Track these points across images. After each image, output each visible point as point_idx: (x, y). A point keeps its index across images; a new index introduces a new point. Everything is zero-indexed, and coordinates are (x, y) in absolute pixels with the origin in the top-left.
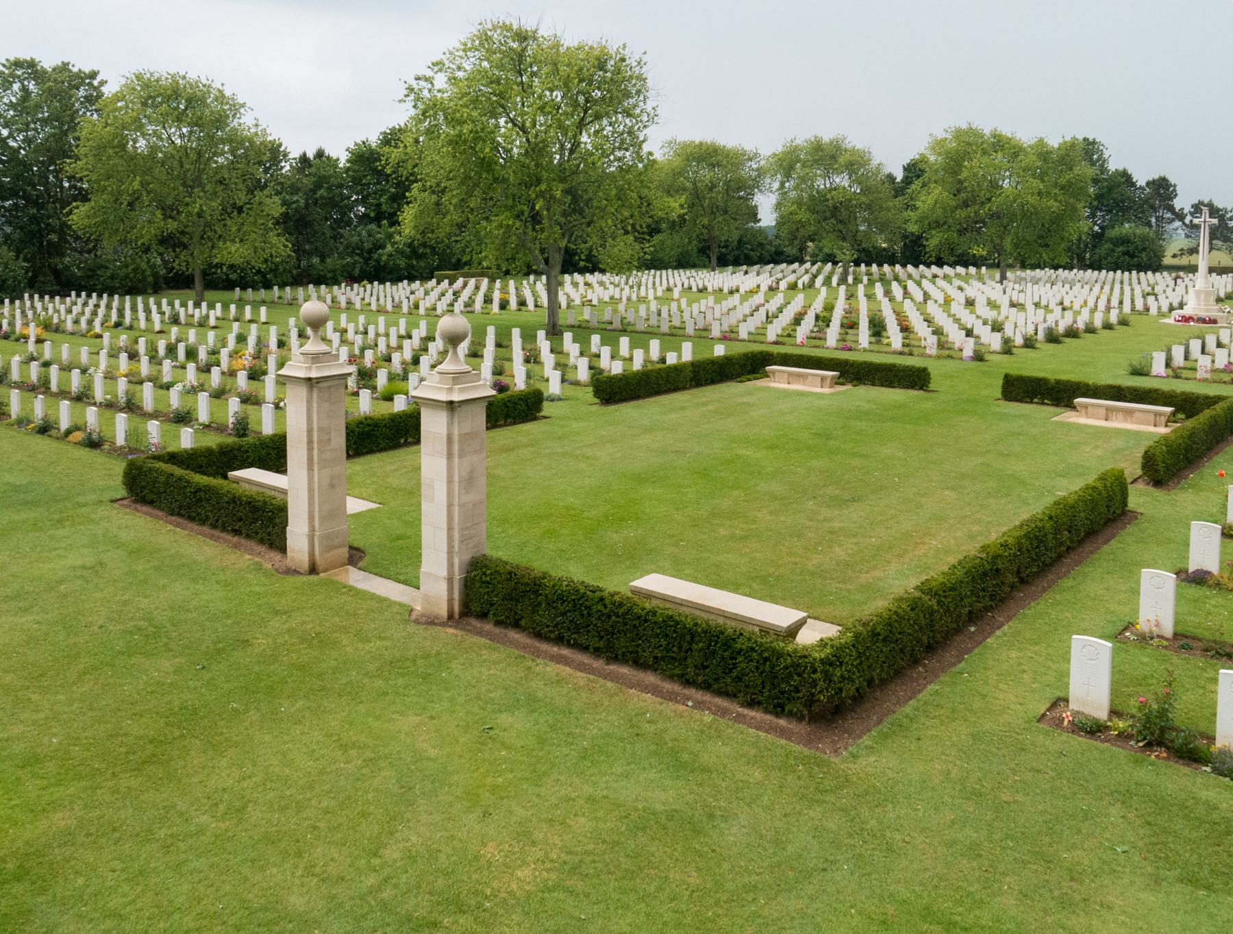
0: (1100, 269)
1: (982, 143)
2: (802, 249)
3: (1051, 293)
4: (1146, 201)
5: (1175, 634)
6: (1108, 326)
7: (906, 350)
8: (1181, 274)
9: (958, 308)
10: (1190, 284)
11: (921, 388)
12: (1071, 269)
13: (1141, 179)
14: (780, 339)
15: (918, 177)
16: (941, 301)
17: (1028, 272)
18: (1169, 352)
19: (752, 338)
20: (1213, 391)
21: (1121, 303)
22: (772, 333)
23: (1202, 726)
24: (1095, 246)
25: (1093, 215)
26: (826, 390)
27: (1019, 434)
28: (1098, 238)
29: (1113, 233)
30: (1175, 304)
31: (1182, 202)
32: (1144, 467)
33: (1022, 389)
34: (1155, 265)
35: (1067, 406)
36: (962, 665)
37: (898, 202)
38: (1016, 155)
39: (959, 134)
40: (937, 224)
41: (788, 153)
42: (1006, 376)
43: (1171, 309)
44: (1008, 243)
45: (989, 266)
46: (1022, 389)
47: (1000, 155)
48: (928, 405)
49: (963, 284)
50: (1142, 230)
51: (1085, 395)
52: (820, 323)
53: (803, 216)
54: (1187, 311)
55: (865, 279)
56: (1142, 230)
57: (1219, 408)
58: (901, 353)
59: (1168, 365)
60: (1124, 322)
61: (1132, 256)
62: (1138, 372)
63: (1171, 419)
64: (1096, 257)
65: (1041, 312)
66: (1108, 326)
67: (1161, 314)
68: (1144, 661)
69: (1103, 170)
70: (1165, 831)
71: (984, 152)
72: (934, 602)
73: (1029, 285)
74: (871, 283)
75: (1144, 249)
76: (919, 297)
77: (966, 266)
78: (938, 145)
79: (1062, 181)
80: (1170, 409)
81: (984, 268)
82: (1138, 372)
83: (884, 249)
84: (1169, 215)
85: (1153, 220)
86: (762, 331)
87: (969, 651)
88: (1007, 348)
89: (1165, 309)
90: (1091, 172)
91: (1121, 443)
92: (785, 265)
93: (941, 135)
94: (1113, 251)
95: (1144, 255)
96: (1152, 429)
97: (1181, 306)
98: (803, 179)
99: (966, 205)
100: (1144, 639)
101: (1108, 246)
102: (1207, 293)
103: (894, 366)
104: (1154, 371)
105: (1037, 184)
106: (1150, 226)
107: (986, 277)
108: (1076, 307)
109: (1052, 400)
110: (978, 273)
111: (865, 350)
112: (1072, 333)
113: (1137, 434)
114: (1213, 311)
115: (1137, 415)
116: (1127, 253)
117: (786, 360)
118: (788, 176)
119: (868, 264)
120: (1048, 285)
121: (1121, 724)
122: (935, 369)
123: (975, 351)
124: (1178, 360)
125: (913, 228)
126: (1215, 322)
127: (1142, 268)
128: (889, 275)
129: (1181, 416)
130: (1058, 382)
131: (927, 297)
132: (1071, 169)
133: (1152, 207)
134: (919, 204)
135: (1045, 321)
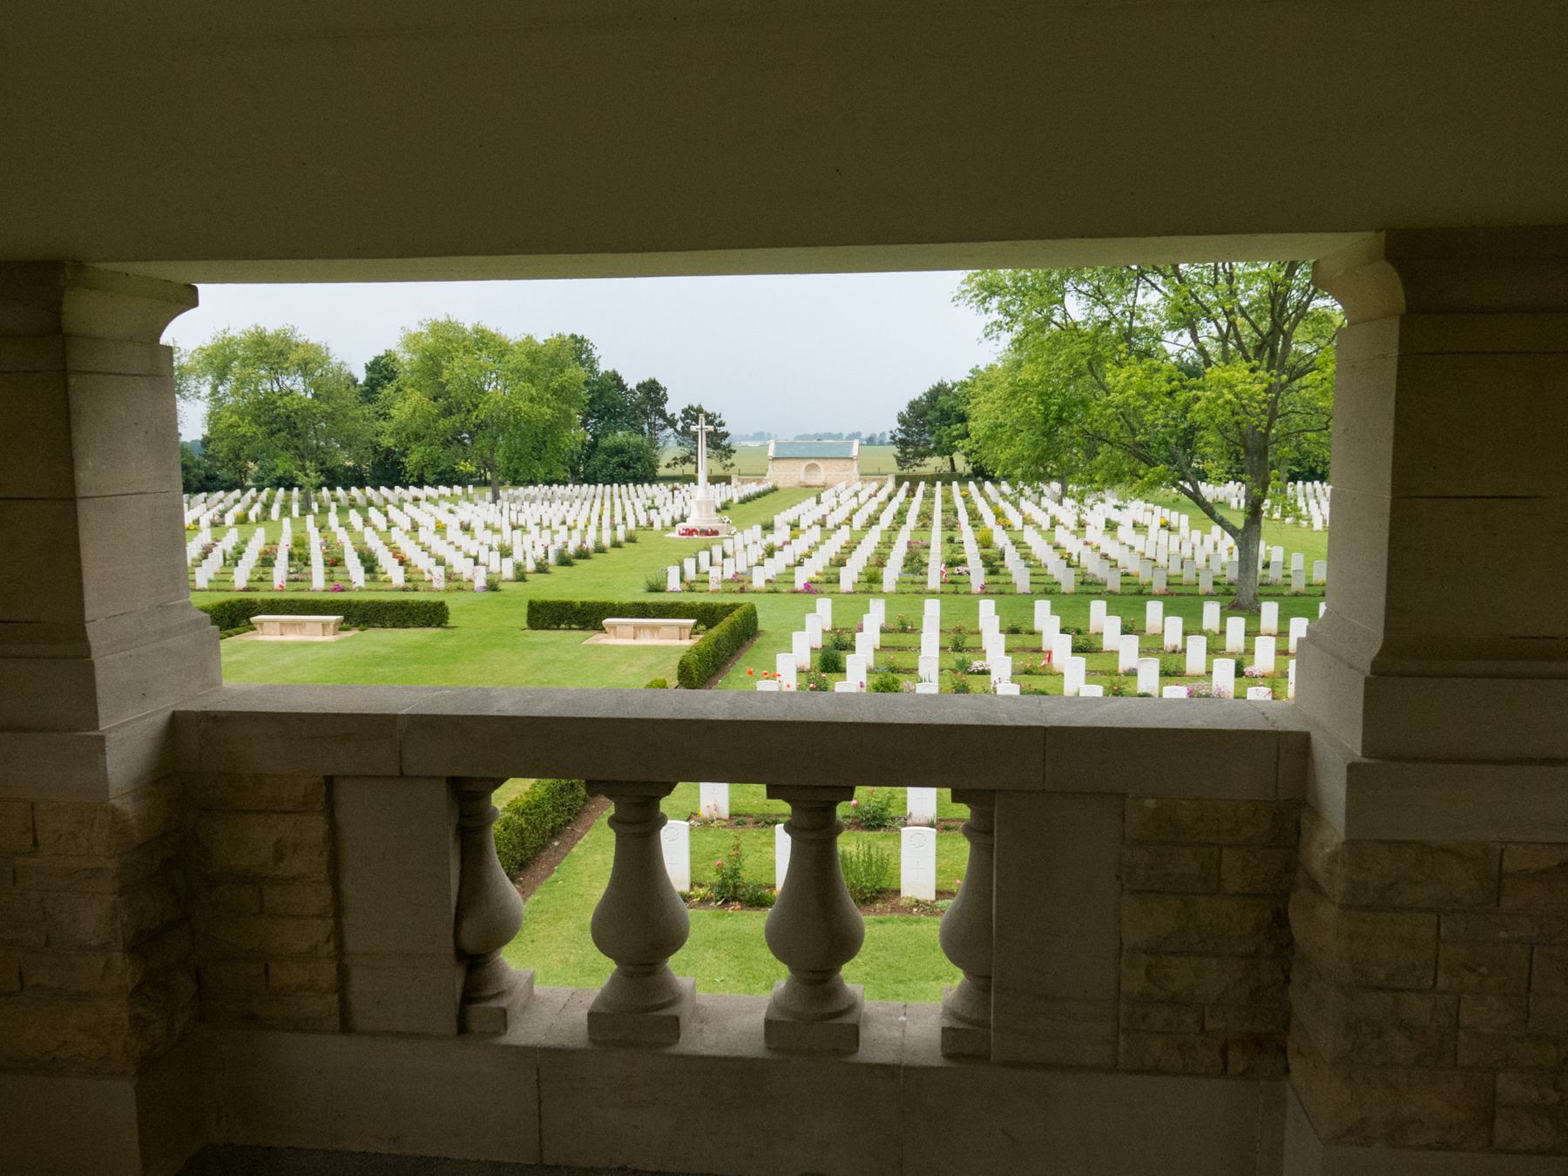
0: (595, 483)
1: (464, 339)
2: (244, 472)
3: (551, 512)
4: (637, 407)
5: (731, 816)
6: (616, 545)
7: (410, 585)
8: (677, 484)
9: (454, 533)
10: (687, 496)
11: (439, 625)
12: (566, 484)
13: (631, 382)
14: (252, 585)
15: (390, 380)
16: (408, 526)
17: (521, 489)
18: (681, 565)
19: (214, 586)
20: (728, 600)
21: (624, 519)
22: (241, 576)
23: (764, 880)
24: (588, 458)
25: (584, 424)
26: (330, 638)
27: (553, 661)
28: (593, 447)
29: (606, 442)
30: (677, 518)
31: (673, 407)
32: (680, 677)
33: (546, 616)
34: (649, 477)
35: (594, 629)
36: (554, 875)
37: (368, 409)
38: (502, 354)
39: (436, 329)
40: (418, 437)
41: (223, 347)
42: (531, 603)
43: (674, 523)
44: (499, 458)
45: (476, 485)
46: (546, 616)
47: (484, 353)
48: (451, 642)
49: (452, 506)
50: (636, 439)
51: (611, 616)
52: (296, 562)
53: (247, 429)
54: (690, 524)
55: (333, 506)
56: (636, 439)
57: (736, 615)
58: (404, 590)
59: (682, 580)
60: (631, 539)
61: (628, 467)
62: (654, 589)
63: (694, 631)
64: (590, 470)
65: (547, 533)
66: (616, 545)
67: (665, 529)
68: (710, 839)
69: (592, 370)
70: (749, 959)
71: (467, 351)
72: (522, 821)
73: (526, 504)
74: (342, 511)
75: (639, 459)
76: (382, 526)
77: (449, 484)
78: (412, 341)
79: (554, 385)
80: (692, 621)
81: (470, 487)
82: (654, 589)
83: (349, 468)
84: (660, 422)
85: (646, 427)
86: (223, 577)
87: (558, 863)
88: (521, 577)
89: (668, 523)
90: (582, 373)
91: (652, 659)
92: (221, 494)
93: (415, 328)
94: (608, 462)
95: (638, 466)
96: (678, 642)
97: (683, 519)
98: (242, 382)
99: (448, 412)
100: (706, 823)
101: (602, 457)
102: (708, 504)
103: (406, 602)
104: (670, 588)
105: (525, 386)
106: (644, 434)
107: (476, 497)
108: (555, 526)
109: (579, 623)
110: (465, 494)
111: (361, 589)
112: (582, 554)
113: (666, 648)
114: (712, 522)
115: (664, 629)
116: (622, 464)
117: (274, 607)
118: (222, 376)
119: (332, 488)
120: (546, 503)
121: (702, 891)
122: (452, 602)
123: (488, 581)
124: (691, 574)
125: (387, 442)
126: (715, 533)
127: (639, 480)
128: (360, 501)
129: (702, 627)
130: (584, 604)
131: (391, 525)
132: (562, 371)
133: (644, 412)
134: (393, 412)
135: (553, 542)
